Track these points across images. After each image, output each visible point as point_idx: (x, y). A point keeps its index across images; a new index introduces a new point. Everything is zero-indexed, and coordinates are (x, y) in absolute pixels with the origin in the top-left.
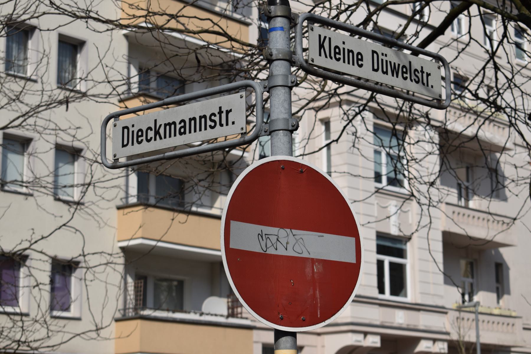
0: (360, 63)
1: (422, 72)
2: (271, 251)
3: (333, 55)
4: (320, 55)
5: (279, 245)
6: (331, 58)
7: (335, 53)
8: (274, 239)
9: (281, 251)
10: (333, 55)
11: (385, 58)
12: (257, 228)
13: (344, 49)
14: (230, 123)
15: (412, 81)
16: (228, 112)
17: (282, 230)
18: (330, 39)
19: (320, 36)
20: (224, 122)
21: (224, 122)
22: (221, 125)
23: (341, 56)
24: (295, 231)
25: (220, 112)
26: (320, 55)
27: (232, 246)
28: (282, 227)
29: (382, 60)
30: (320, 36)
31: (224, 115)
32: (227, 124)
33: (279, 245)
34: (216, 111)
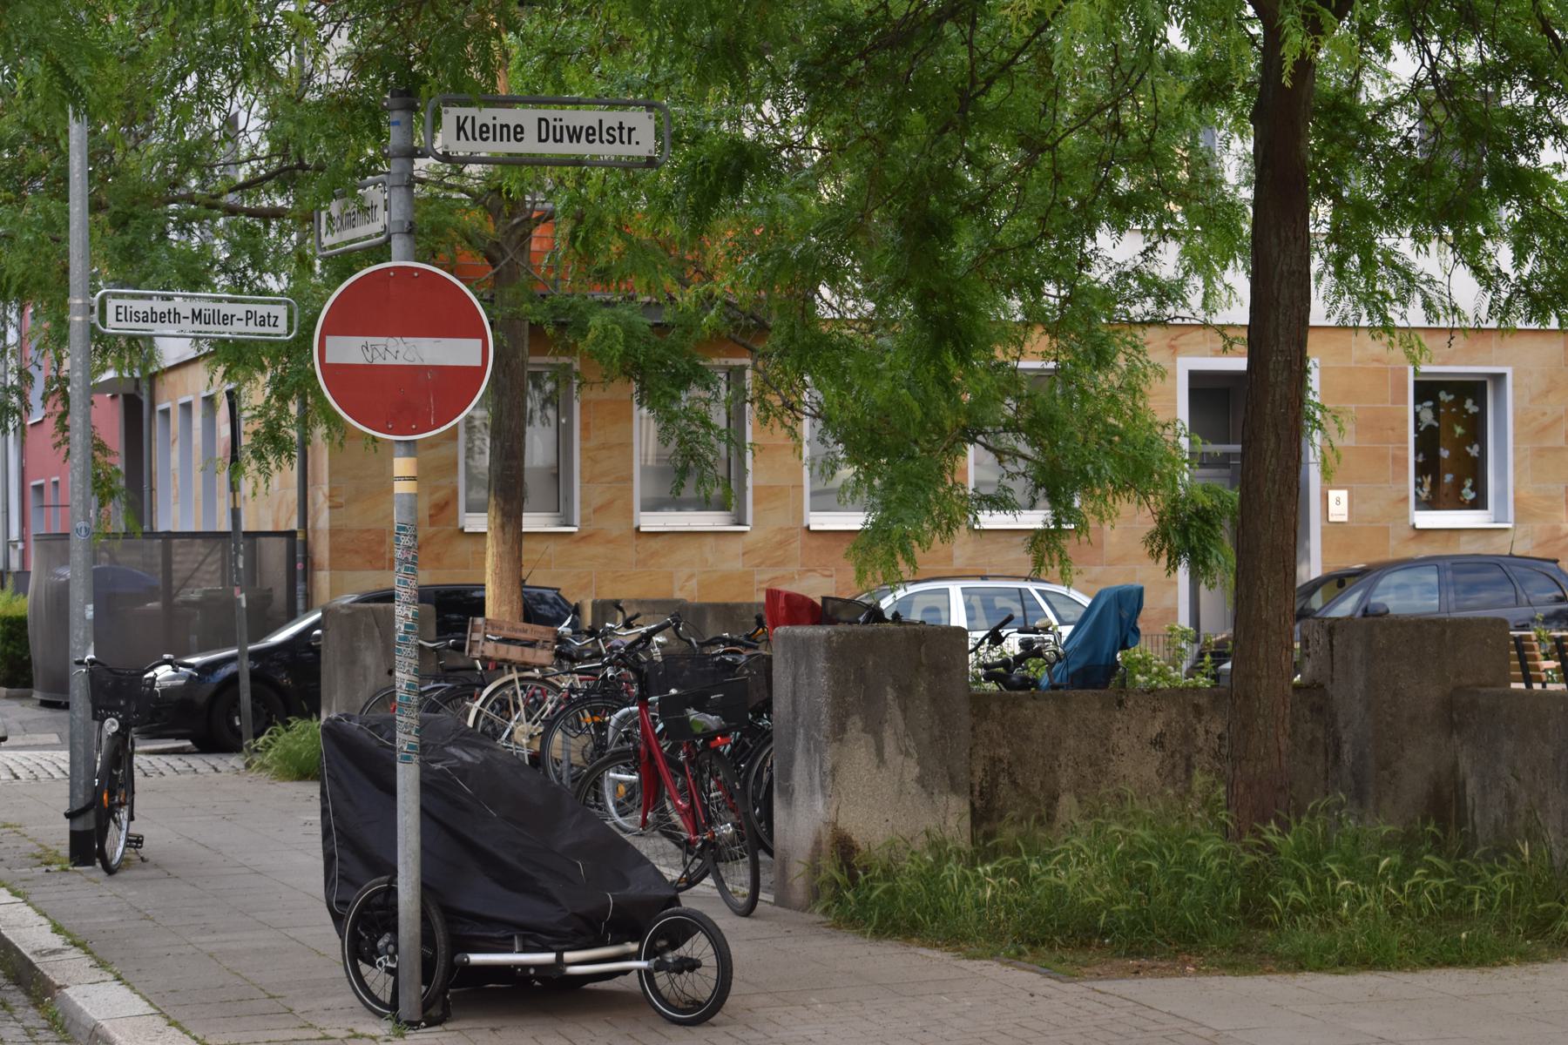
0: (519, 136)
1: (621, 128)
2: (379, 361)
3: (477, 135)
4: (458, 139)
5: (388, 355)
6: (475, 139)
7: (481, 132)
8: (382, 349)
9: (390, 361)
10: (477, 135)
11: (558, 124)
12: (361, 340)
13: (494, 126)
14: (633, 141)
15: (602, 142)
16: (630, 130)
17: (391, 340)
18: (473, 118)
19: (458, 118)
20: (625, 138)
21: (625, 138)
22: (622, 142)
23: (491, 135)
24: (405, 339)
25: (621, 128)
26: (458, 139)
27: (328, 360)
28: (392, 336)
29: (555, 127)
30: (458, 118)
31: (625, 132)
32: (630, 142)
33: (388, 355)
34: (616, 126)
